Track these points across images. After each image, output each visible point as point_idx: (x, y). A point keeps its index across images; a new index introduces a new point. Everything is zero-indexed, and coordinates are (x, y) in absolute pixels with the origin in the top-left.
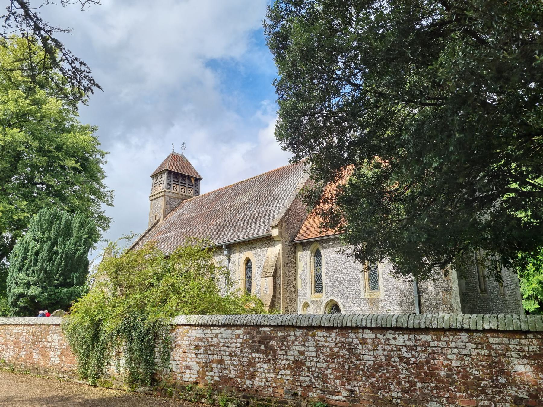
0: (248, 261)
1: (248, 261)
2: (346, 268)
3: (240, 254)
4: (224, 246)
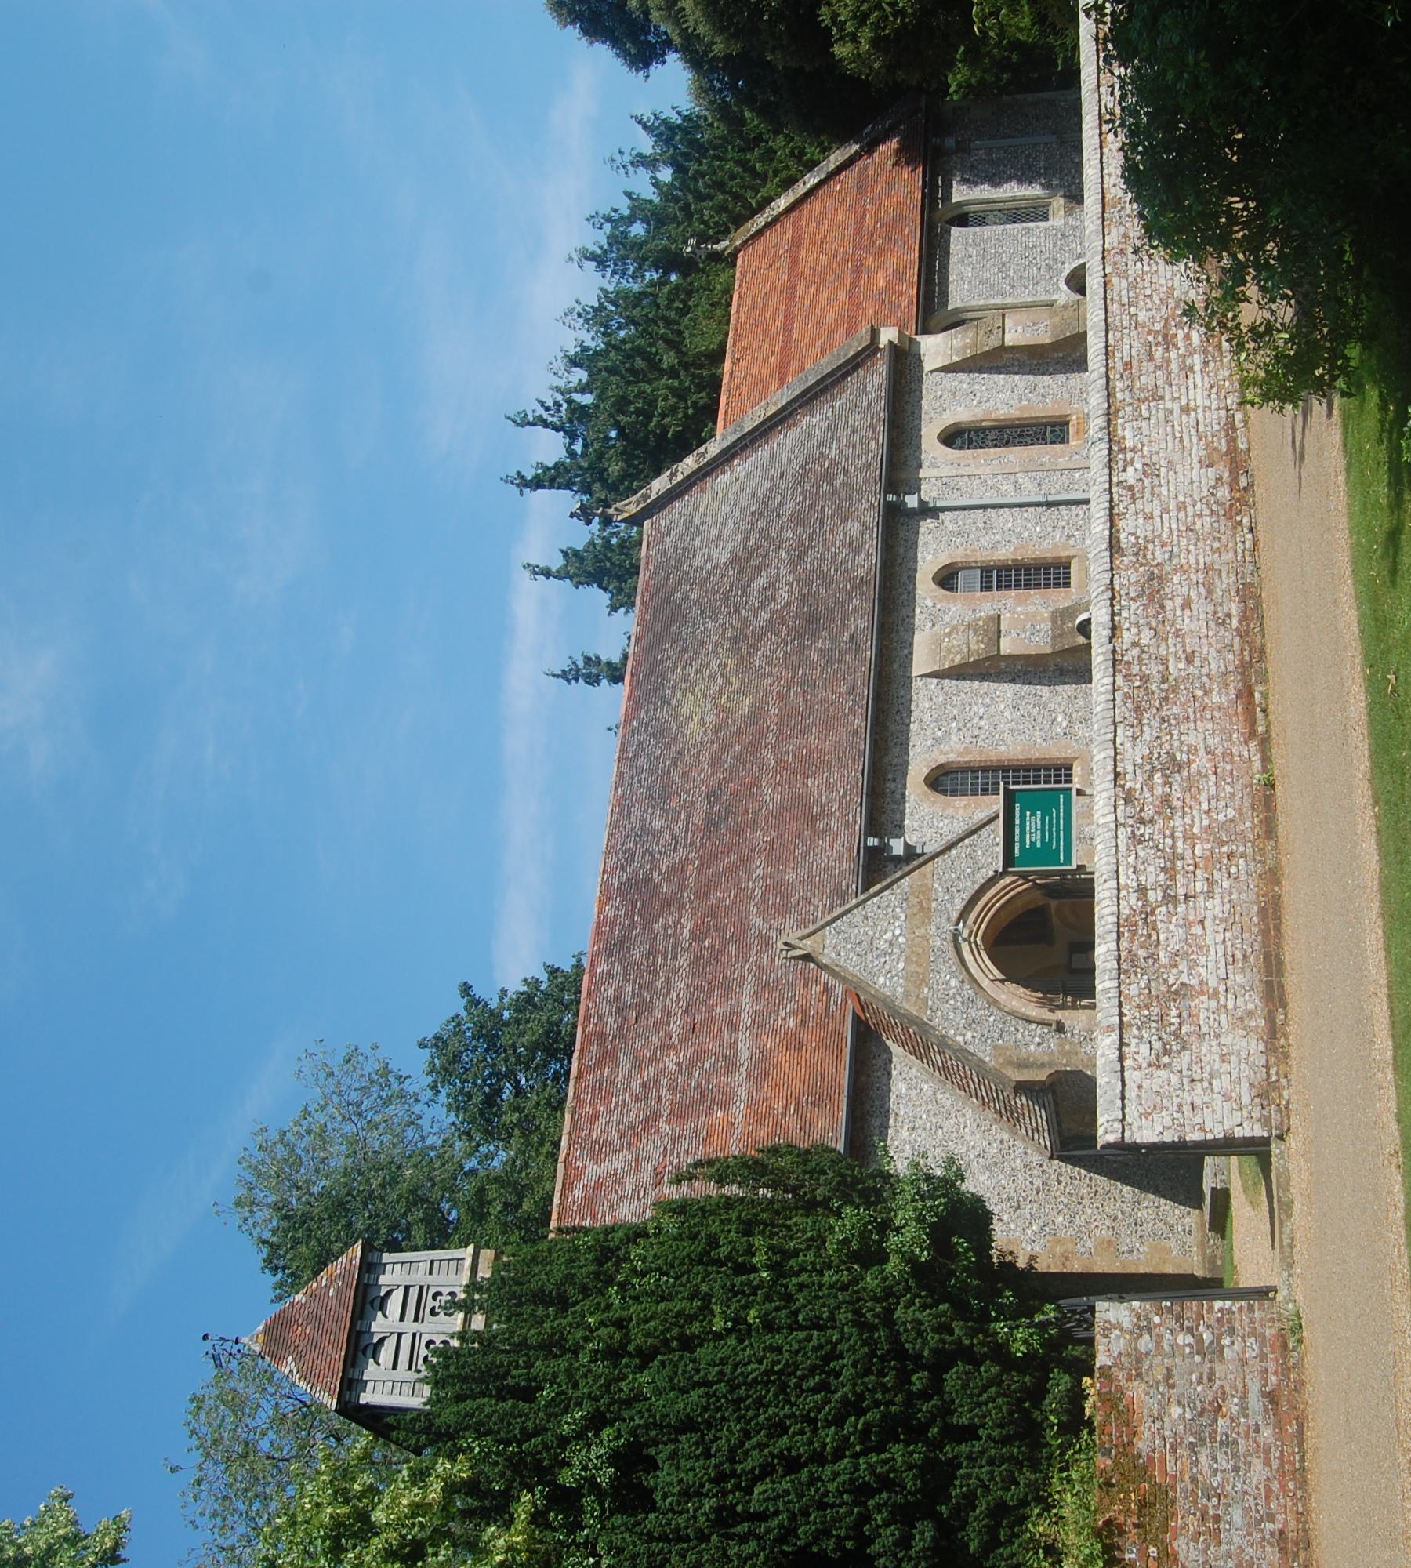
0: (953, 437)
1: (953, 437)
2: (998, 255)
3: (926, 464)
4: (891, 498)
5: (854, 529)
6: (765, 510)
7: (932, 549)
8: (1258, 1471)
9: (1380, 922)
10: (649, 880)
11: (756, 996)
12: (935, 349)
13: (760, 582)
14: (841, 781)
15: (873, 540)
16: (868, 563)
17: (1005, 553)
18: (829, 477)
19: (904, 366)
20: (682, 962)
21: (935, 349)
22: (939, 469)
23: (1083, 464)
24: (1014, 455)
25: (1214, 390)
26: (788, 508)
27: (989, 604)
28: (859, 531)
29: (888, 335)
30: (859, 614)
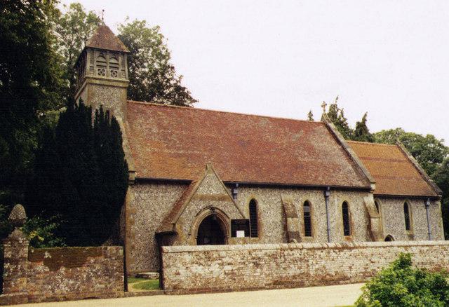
7: (315, 198)
12: (370, 200)
15: (318, 184)
17: (314, 219)
19: (367, 190)
21: (370, 200)
22: (337, 200)
23: (338, 238)
24: (341, 221)
27: (300, 214)
28: (322, 181)
29: (373, 187)
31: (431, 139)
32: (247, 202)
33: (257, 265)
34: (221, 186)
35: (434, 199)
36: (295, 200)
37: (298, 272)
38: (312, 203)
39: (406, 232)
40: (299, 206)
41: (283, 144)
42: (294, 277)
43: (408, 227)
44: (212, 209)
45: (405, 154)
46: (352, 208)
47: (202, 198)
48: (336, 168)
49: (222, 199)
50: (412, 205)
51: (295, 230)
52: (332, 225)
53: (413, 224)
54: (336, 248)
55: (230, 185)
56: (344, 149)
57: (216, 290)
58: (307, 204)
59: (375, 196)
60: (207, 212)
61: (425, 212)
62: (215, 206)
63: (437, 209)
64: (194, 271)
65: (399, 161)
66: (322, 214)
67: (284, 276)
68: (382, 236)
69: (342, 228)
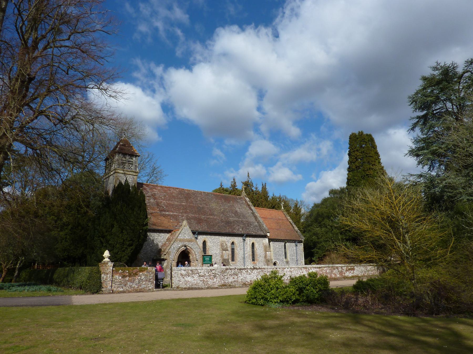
5: (241, 230)
6: (244, 216)
7: (238, 240)
8: (136, 286)
9: (297, 276)
10: (191, 198)
11: (175, 215)
12: (267, 240)
13: (233, 215)
14: (205, 228)
15: (239, 233)
16: (236, 232)
17: (236, 251)
18: (248, 226)
19: (265, 236)
20: (179, 203)
22: (249, 241)
23: (249, 264)
24: (251, 253)
25: (143, 329)
26: (244, 220)
27: (230, 249)
28: (241, 231)
29: (268, 234)
30: (228, 230)
31: (353, 134)
32: (202, 242)
33: (215, 276)
34: (191, 234)
35: (300, 242)
36: (228, 240)
37: (233, 280)
38: (236, 243)
39: (284, 260)
40: (229, 245)
41: (221, 209)
42: (231, 282)
43: (286, 258)
44: (185, 246)
45: (286, 217)
46: (256, 246)
47: (180, 241)
48: (249, 224)
49: (190, 241)
50: (287, 244)
51: (226, 258)
52: (246, 255)
53: (288, 255)
54: (251, 269)
55: (194, 233)
56: (253, 213)
57: (196, 289)
58: (233, 243)
59: (269, 239)
60: (183, 248)
61: (295, 249)
62: (187, 245)
63: (301, 247)
64: (186, 279)
65: (283, 220)
66: (341, 273)
67: (226, 282)
68: (272, 262)
69: (251, 257)
